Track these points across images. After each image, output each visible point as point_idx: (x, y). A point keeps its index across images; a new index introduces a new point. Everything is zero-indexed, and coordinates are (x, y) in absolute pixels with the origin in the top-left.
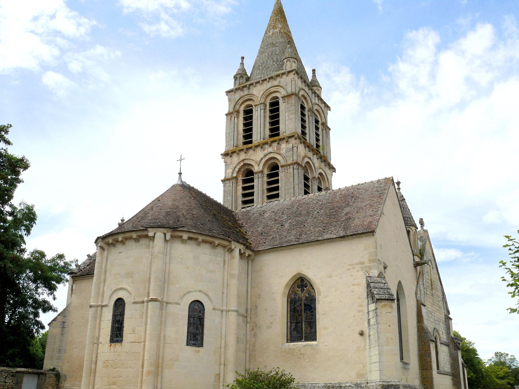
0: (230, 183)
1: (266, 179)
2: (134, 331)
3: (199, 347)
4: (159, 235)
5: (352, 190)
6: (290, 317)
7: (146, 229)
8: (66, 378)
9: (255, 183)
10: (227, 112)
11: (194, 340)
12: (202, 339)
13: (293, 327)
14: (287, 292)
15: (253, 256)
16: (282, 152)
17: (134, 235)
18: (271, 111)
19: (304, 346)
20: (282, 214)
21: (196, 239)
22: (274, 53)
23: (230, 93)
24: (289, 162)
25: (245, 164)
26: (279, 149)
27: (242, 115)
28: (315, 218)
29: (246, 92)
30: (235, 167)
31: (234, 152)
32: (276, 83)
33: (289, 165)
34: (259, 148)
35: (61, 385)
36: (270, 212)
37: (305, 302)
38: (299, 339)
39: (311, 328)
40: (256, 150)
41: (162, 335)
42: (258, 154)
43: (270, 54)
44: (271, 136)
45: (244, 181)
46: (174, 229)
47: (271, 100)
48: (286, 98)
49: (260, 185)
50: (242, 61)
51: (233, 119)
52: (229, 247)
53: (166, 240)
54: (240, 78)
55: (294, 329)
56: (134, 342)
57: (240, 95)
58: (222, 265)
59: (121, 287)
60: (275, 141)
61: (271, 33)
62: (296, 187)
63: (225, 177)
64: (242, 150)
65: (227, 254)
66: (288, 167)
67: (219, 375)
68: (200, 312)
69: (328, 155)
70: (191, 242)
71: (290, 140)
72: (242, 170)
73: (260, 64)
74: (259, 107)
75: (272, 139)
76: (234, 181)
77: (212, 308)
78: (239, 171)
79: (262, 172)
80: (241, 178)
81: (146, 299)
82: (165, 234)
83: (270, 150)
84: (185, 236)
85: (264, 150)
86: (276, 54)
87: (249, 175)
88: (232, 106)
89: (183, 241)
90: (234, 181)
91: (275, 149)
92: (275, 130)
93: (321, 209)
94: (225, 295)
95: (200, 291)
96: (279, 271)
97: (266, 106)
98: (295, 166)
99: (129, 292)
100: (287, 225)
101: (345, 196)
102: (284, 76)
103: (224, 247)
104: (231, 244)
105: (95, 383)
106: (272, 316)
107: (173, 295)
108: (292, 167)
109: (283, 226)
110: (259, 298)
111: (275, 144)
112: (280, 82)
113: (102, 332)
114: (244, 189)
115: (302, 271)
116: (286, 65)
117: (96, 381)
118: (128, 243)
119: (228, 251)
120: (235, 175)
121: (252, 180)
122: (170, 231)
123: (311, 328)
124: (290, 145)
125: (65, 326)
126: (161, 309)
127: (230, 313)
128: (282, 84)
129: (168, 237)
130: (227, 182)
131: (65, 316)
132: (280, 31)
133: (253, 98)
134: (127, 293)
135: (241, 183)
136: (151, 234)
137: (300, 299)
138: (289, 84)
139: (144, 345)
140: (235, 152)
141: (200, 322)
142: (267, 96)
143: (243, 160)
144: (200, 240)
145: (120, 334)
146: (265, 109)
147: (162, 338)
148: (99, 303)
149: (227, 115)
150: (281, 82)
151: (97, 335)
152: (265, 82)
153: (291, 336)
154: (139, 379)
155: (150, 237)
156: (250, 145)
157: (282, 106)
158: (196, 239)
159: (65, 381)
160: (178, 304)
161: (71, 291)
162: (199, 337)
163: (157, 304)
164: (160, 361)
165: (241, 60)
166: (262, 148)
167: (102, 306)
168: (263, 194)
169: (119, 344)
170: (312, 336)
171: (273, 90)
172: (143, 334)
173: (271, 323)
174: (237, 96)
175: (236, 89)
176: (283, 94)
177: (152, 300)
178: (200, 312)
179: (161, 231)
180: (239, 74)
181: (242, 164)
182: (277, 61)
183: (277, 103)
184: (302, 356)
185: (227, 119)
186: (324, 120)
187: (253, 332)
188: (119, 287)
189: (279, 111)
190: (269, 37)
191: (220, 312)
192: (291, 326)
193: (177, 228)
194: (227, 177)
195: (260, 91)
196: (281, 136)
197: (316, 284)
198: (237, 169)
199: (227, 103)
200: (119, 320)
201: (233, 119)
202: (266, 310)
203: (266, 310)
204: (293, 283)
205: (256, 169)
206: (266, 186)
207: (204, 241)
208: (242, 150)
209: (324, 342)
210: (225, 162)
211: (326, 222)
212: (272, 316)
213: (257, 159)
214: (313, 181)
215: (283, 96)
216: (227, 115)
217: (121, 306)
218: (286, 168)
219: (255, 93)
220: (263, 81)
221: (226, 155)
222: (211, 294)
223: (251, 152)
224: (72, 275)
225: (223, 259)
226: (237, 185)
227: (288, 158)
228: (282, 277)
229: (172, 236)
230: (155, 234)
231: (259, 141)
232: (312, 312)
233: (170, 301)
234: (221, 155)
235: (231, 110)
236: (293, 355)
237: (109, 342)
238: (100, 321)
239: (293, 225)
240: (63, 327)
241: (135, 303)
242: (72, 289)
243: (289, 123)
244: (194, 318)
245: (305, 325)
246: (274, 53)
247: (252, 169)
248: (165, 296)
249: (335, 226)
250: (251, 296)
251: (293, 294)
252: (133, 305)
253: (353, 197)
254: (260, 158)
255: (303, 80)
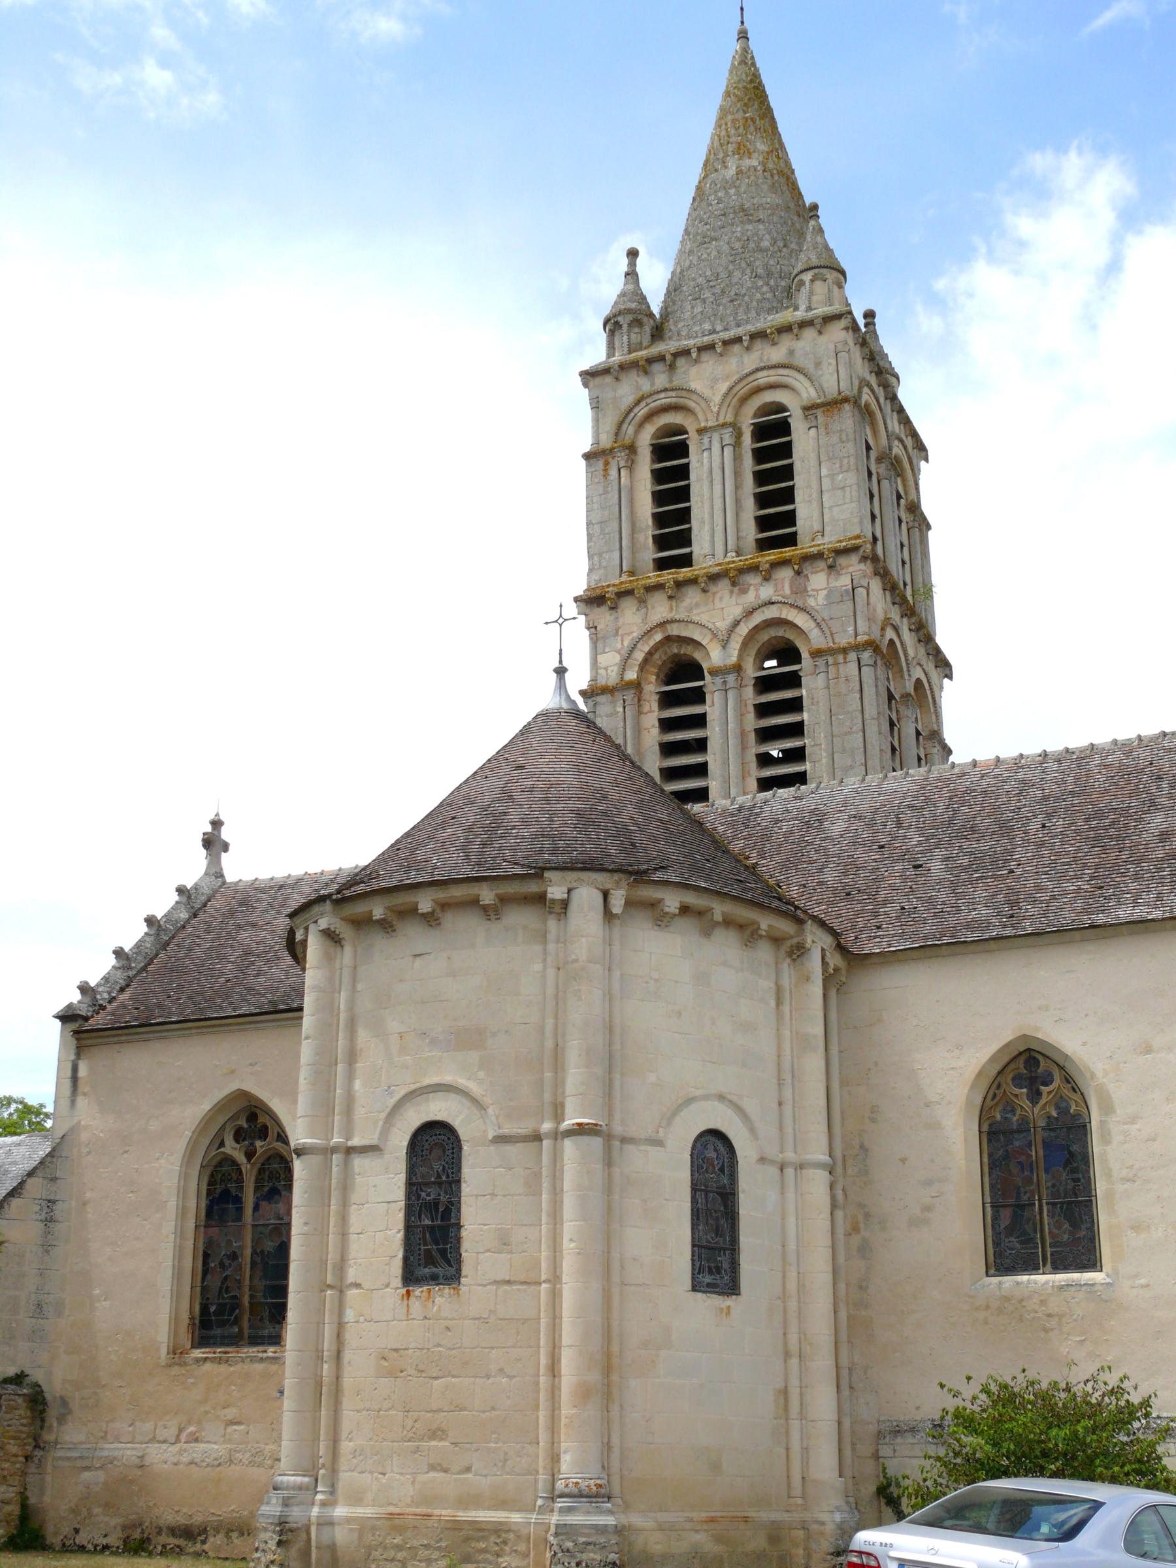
0: (614, 703)
1: (750, 696)
2: (504, 1242)
3: (729, 1295)
4: (586, 895)
5: (1144, 755)
6: (992, 1187)
7: (539, 873)
8: (70, 1412)
9: (712, 708)
10: (587, 448)
11: (710, 1272)
12: (735, 1266)
13: (1005, 1221)
14: (978, 1100)
15: (844, 972)
16: (811, 602)
17: (487, 895)
18: (760, 455)
19: (1061, 1288)
20: (899, 823)
21: (700, 913)
22: (752, 245)
23: (598, 380)
24: (843, 640)
25: (668, 639)
26: (801, 591)
27: (645, 465)
28: (1040, 845)
29: (661, 379)
30: (633, 648)
31: (622, 594)
32: (776, 354)
33: (844, 651)
34: (724, 585)
35: (51, 1437)
36: (844, 816)
37: (1046, 1134)
38: (1030, 1265)
39: (1075, 1225)
40: (713, 589)
41: (615, 1255)
42: (718, 604)
43: (737, 245)
44: (764, 545)
45: (668, 700)
46: (638, 876)
47: (755, 416)
48: (819, 412)
49: (728, 717)
50: (632, 264)
51: (613, 472)
52: (795, 941)
53: (608, 914)
54: (630, 325)
55: (1010, 1230)
56: (508, 1282)
57: (638, 388)
58: (773, 1003)
59: (436, 1080)
60: (785, 563)
61: (732, 171)
62: (872, 729)
63: (593, 679)
64: (659, 587)
65: (785, 965)
66: (840, 658)
67: (785, 1392)
68: (722, 1170)
69: (929, 618)
70: (686, 923)
71: (842, 561)
72: (658, 658)
73: (701, 280)
74: (716, 437)
75: (773, 555)
76: (630, 696)
77: (755, 1157)
78: (646, 661)
79: (738, 668)
80: (652, 688)
81: (547, 1126)
82: (606, 895)
83: (767, 592)
84: (672, 901)
85: (744, 591)
86: (761, 250)
87: (680, 676)
88: (609, 425)
89: (661, 919)
90: (630, 696)
91: (787, 591)
92: (776, 522)
93: (1049, 816)
94: (788, 1110)
95: (721, 1097)
96: (946, 1032)
97: (739, 435)
98: (866, 656)
99: (474, 1101)
100: (936, 867)
101: (1124, 772)
102: (809, 334)
103: (776, 940)
104: (801, 932)
105: (344, 1435)
106: (929, 1183)
107: (638, 1117)
108: (853, 656)
109: (920, 871)
110: (873, 1120)
111: (786, 574)
112: (791, 352)
113: (358, 1249)
114: (667, 725)
115: (1037, 1029)
116: (811, 293)
117: (346, 1426)
118: (449, 920)
119: (790, 954)
120: (632, 675)
121: (698, 696)
122: (624, 884)
123: (1075, 1225)
124: (844, 581)
125: (57, 1214)
126: (609, 1163)
127: (809, 1173)
128: (799, 361)
129: (617, 903)
130: (601, 699)
131: (54, 1179)
132: (764, 164)
133: (691, 404)
134: (468, 1103)
135: (655, 706)
136: (556, 892)
137: (1024, 1127)
138: (825, 364)
139: (555, 1296)
140: (629, 593)
141: (726, 1207)
142: (744, 400)
143: (662, 625)
144: (718, 917)
145: (443, 1253)
146: (737, 444)
147: (616, 1266)
148: (337, 1140)
149: (587, 457)
150: (798, 354)
151: (332, 1256)
152: (736, 348)
153: (998, 1254)
154: (542, 1415)
155: (553, 901)
156: (684, 573)
157: (804, 441)
158: (700, 913)
159: (61, 1420)
160: (659, 1143)
161: (67, 1084)
162: (724, 1261)
163: (596, 1142)
164: (615, 1348)
165: (625, 261)
166: (734, 584)
167: (350, 1151)
168: (744, 747)
169: (447, 1290)
170: (1080, 1252)
171: (764, 378)
172: (545, 1254)
173: (928, 1209)
174: (627, 390)
175: (623, 367)
176: (804, 395)
177: (581, 1130)
178: (722, 1170)
179: (593, 884)
180: (629, 311)
181: (658, 637)
182: (769, 274)
183: (783, 427)
184: (1054, 1322)
185: (590, 474)
186: (913, 496)
187: (856, 1240)
188: (427, 1081)
189: (790, 456)
190: (726, 185)
191: (774, 1171)
192: (995, 1219)
193: (646, 872)
194: (602, 682)
195: (715, 381)
196: (805, 545)
197: (1093, 1075)
198: (639, 656)
199: (587, 413)
200: (436, 1204)
201: (613, 472)
202: (903, 1160)
203: (903, 1160)
204: (998, 1068)
205: (715, 656)
206: (752, 722)
207: (728, 923)
208: (659, 587)
209: (1136, 1276)
210: (592, 627)
211: (1090, 860)
212: (929, 1183)
213: (718, 622)
214: (902, 709)
215: (805, 403)
216: (587, 457)
217: (437, 1152)
218: (831, 660)
219: (694, 385)
220: (726, 343)
221: (592, 600)
222: (751, 1106)
223: (692, 596)
224: (74, 1026)
225: (773, 985)
226: (640, 713)
227: (835, 626)
228: (960, 1047)
229: (629, 903)
230: (569, 891)
231: (720, 557)
232: (1075, 1170)
233: (633, 1131)
234: (576, 599)
235: (606, 441)
236: (1021, 1319)
237: (397, 1282)
238: (345, 1203)
239: (963, 868)
240: (49, 1220)
241: (501, 1139)
242: (75, 1079)
243: (828, 500)
244: (706, 1192)
245: (1051, 1215)
246: (752, 245)
247: (698, 656)
248: (617, 1116)
249: (1136, 878)
250: (842, 1113)
251: (1000, 1108)
252: (492, 1148)
253: (1159, 778)
254: (729, 620)
255: (867, 350)
